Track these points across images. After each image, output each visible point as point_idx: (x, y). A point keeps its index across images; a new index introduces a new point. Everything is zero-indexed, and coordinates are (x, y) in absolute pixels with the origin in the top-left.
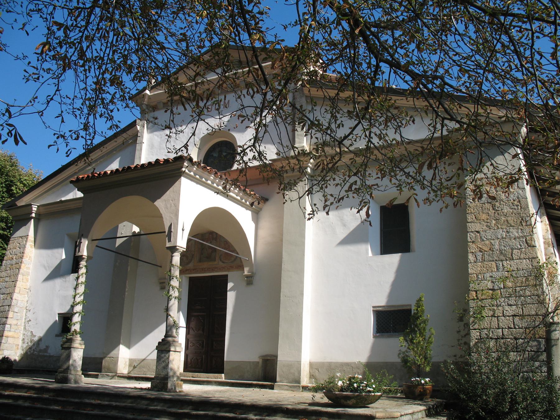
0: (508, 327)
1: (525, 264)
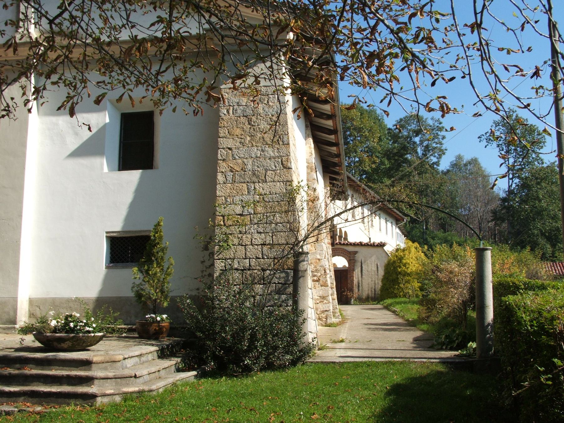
0: (256, 257)
1: (279, 188)
